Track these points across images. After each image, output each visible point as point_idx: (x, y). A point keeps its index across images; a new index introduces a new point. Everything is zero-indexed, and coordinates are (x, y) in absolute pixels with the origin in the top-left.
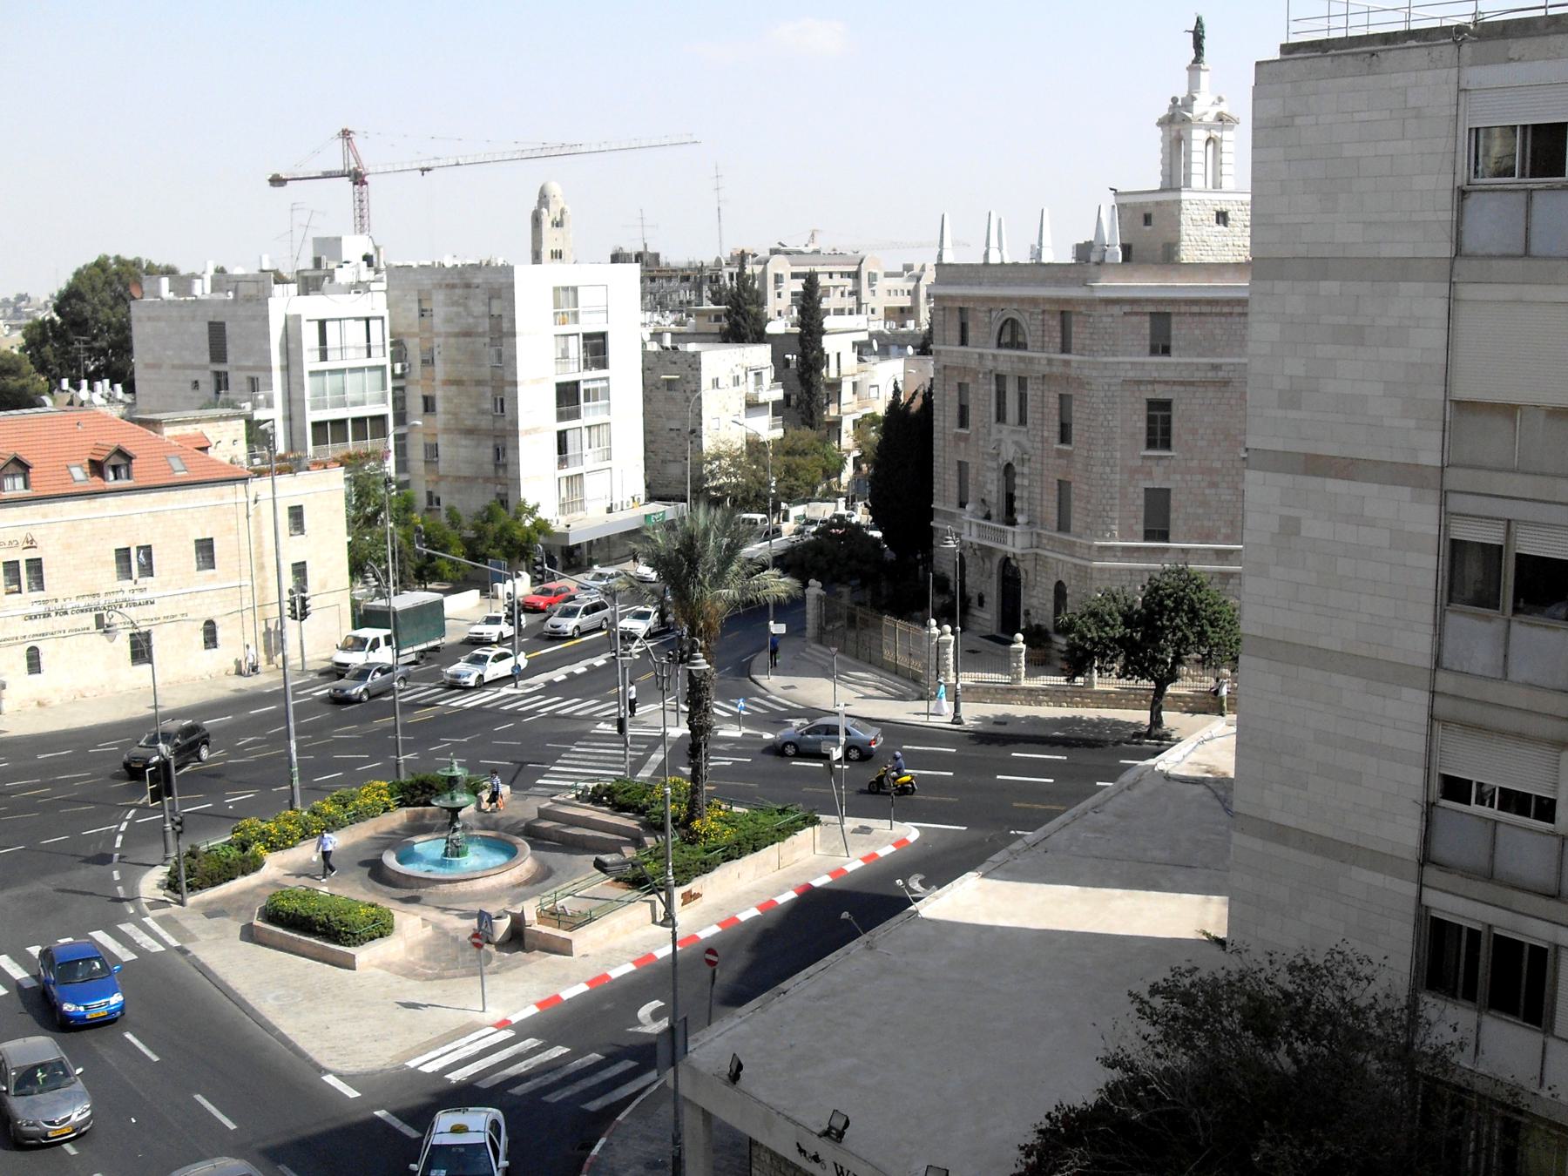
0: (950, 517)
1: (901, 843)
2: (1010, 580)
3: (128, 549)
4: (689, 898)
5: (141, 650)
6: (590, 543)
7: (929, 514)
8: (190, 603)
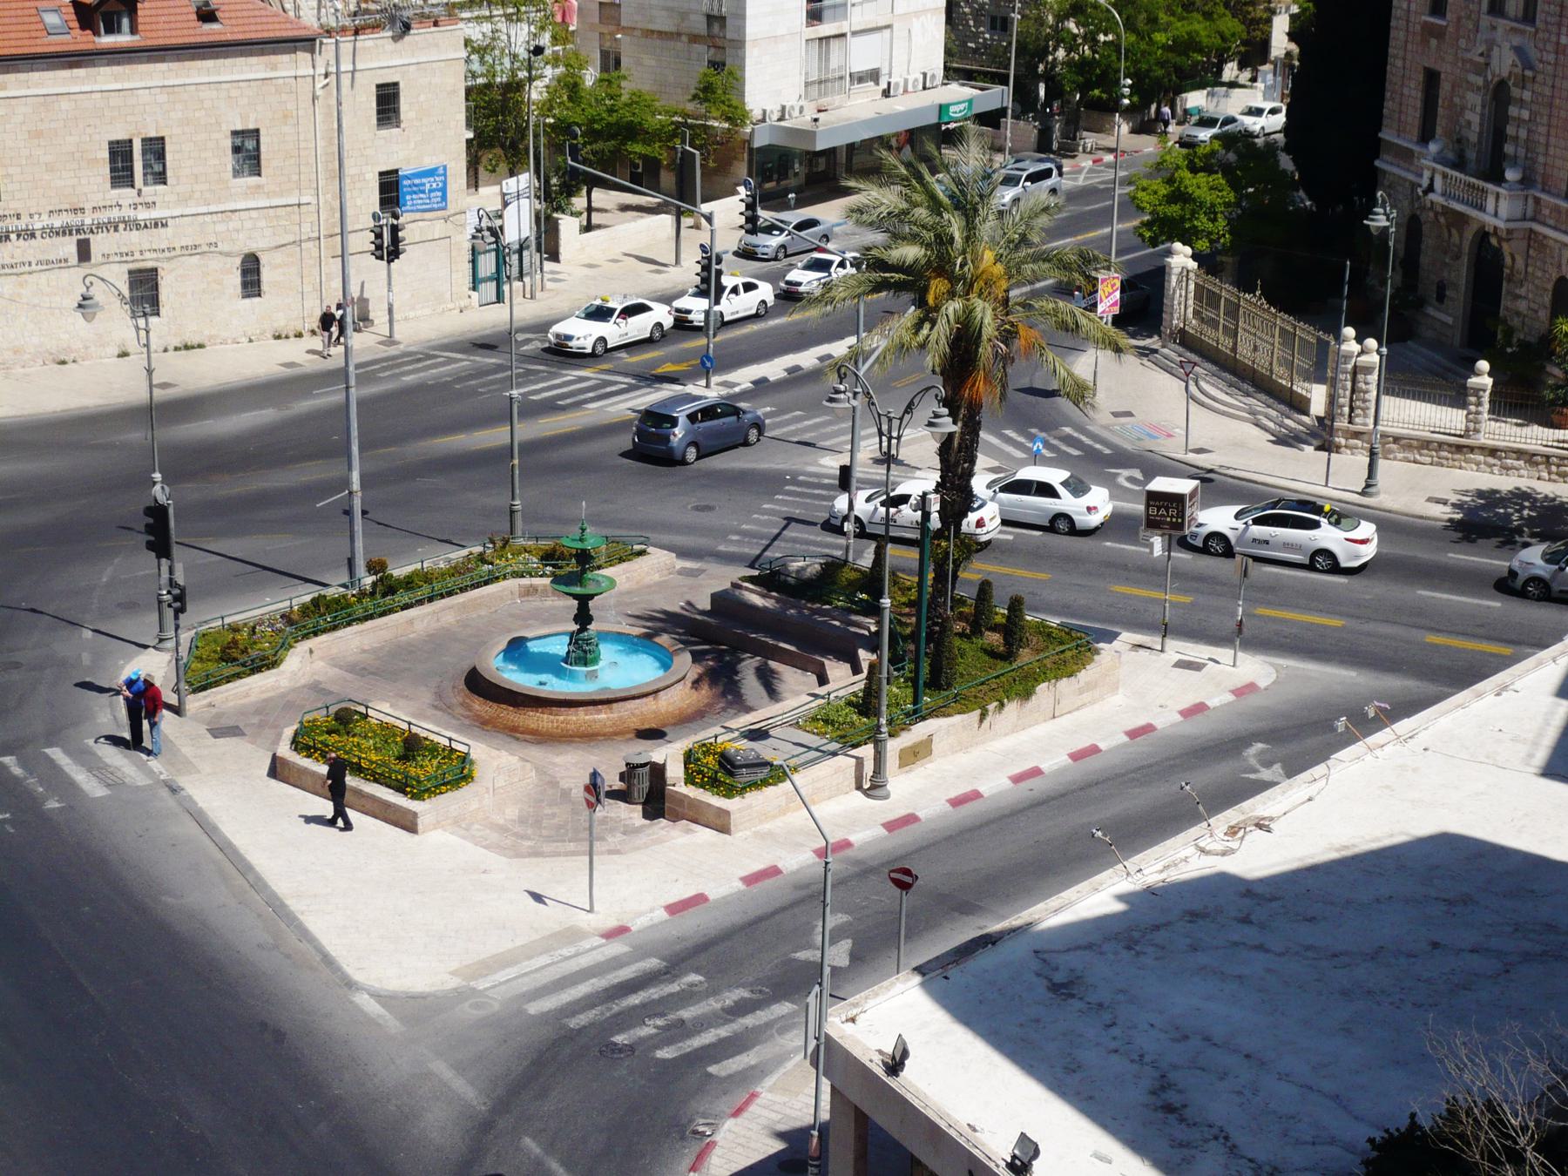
0: (1406, 156)
1: (1248, 689)
2: (1488, 265)
4: (912, 756)
5: (145, 290)
6: (851, 147)
7: (1375, 147)
8: (220, 228)
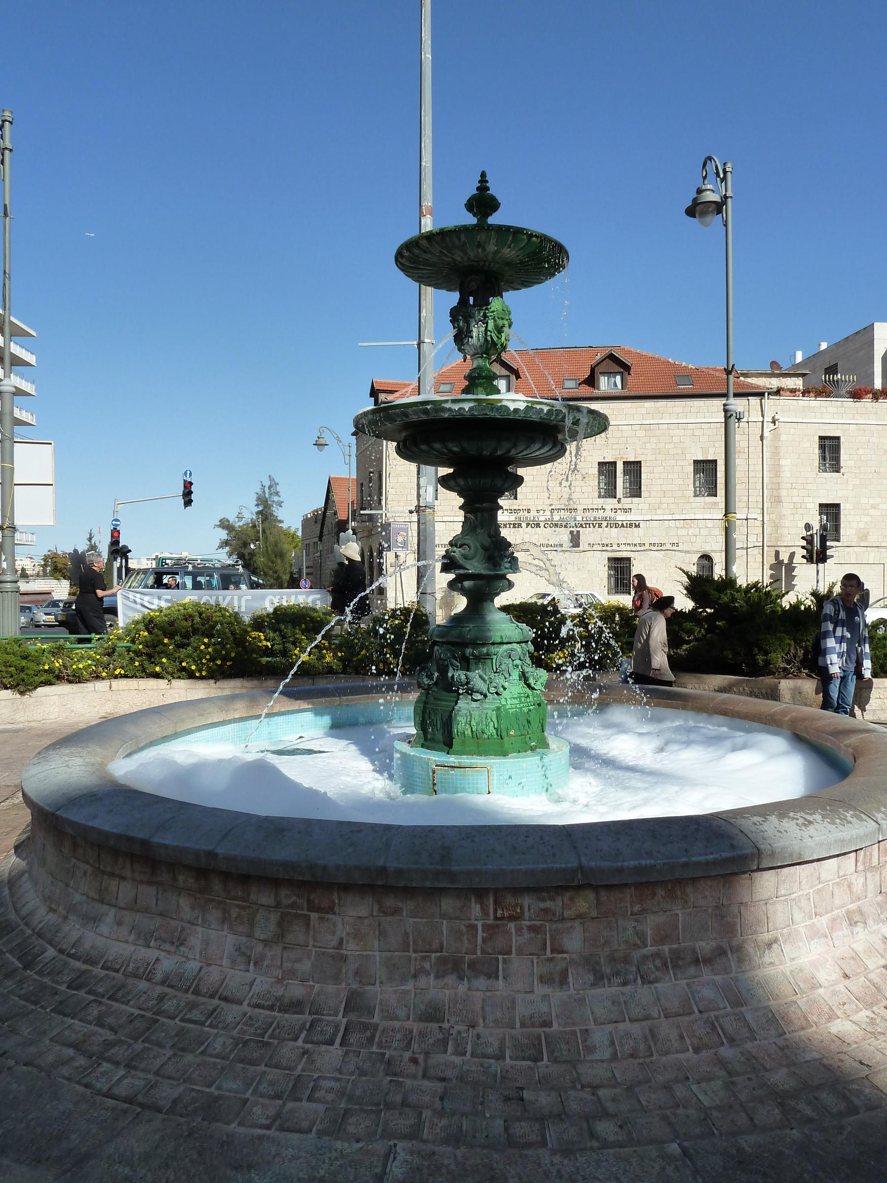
3: (614, 464)
